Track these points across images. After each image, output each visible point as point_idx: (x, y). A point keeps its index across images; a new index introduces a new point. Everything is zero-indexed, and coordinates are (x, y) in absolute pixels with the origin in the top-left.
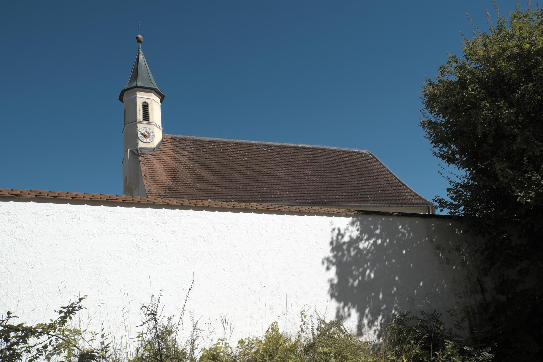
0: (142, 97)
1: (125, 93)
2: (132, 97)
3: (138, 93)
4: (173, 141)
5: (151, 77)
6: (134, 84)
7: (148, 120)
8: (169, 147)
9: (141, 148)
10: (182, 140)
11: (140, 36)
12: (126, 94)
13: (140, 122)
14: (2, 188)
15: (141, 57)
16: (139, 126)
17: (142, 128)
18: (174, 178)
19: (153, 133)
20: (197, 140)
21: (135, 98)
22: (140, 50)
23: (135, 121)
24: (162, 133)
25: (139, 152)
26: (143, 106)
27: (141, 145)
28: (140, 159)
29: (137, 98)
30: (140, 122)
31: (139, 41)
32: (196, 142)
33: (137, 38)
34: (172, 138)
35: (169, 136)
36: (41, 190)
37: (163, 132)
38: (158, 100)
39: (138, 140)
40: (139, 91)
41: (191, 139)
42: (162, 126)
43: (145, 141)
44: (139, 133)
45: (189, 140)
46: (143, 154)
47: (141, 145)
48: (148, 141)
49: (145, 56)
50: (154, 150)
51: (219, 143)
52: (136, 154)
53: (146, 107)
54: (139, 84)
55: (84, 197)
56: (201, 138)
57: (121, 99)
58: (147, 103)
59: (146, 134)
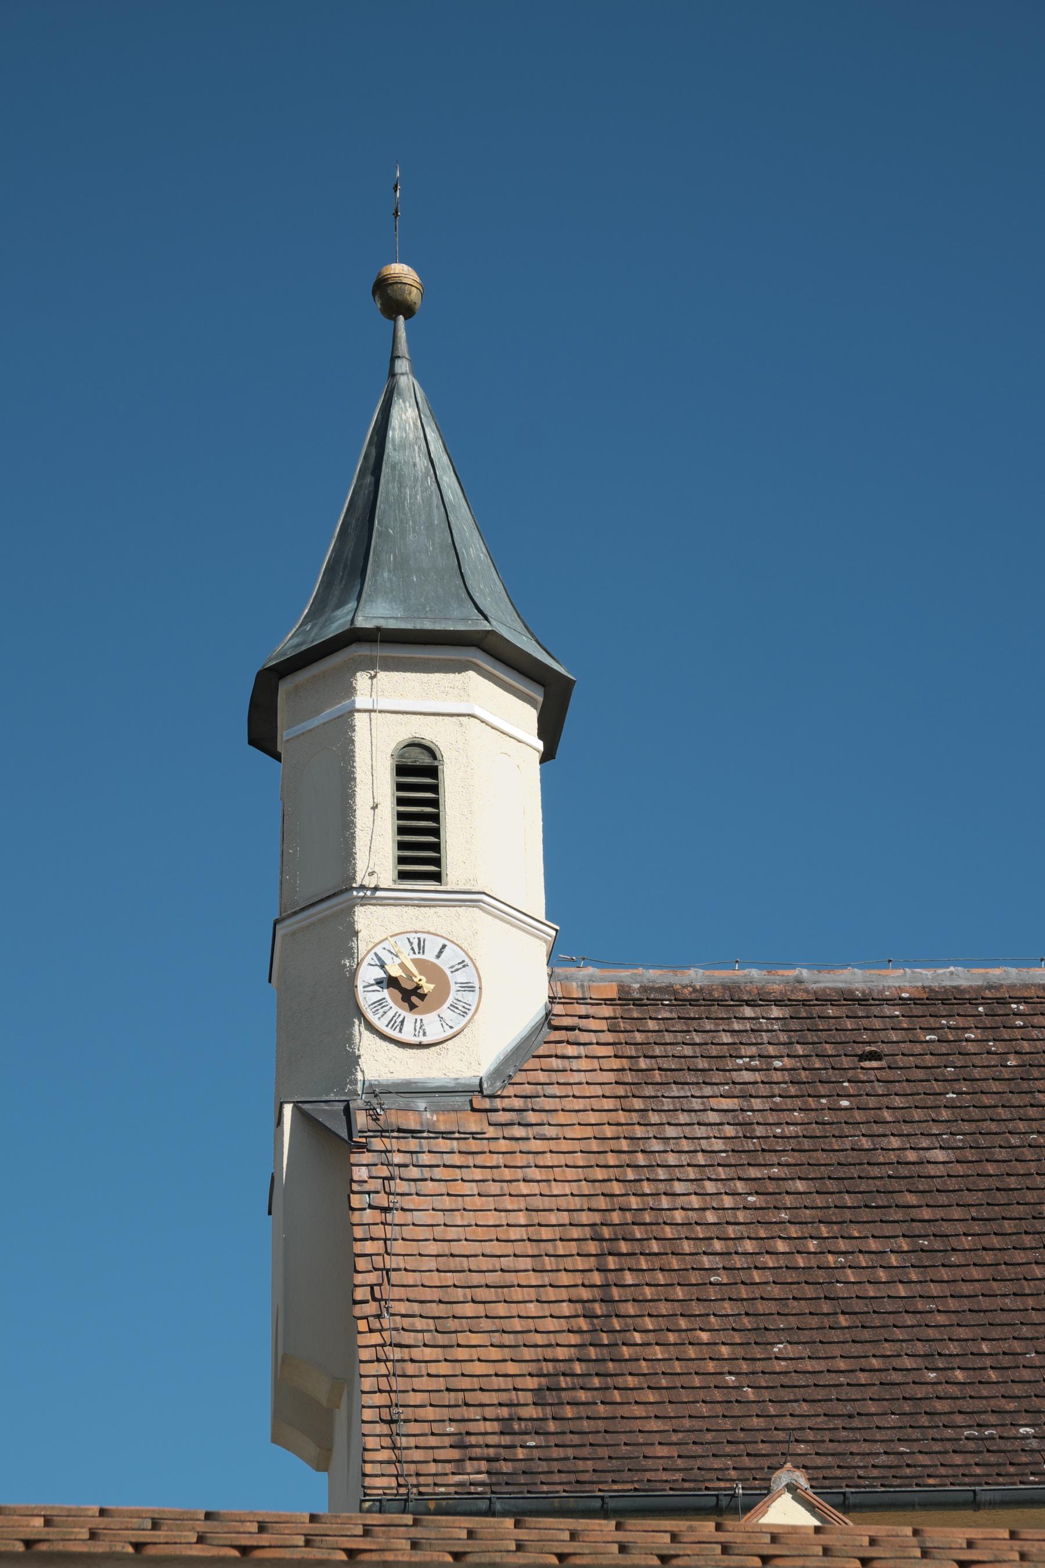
0: (389, 708)
1: (284, 687)
2: (329, 713)
3: (362, 680)
4: (640, 1028)
5: (475, 551)
6: (338, 624)
7: (437, 877)
8: (590, 1067)
9: (377, 1091)
10: (702, 1000)
11: (400, 270)
12: (282, 702)
13: (372, 895)
14: (3, 1504)
15: (405, 416)
16: (370, 922)
17: (384, 934)
18: (601, 1311)
19: (473, 963)
20: (823, 999)
21: (344, 724)
22: (402, 366)
23: (341, 892)
24: (552, 959)
25: (361, 1120)
26: (401, 770)
27: (377, 1063)
28: (360, 1173)
29: (360, 721)
30: (372, 895)
31: (391, 302)
32: (806, 1010)
33: (383, 287)
34: (624, 998)
35: (601, 980)
36: (266, 1510)
37: (557, 957)
38: (520, 717)
39: (358, 1028)
40: (370, 665)
41: (776, 988)
42: (551, 913)
43: (407, 1036)
44: (368, 974)
45: (761, 1000)
46: (382, 1133)
47: (377, 1063)
48: (434, 1031)
49: (442, 410)
50: (475, 1096)
51: (997, 1002)
52: (334, 1134)
53: (419, 776)
54: (376, 612)
55: (623, 1548)
56: (854, 978)
57: (263, 734)
58: (430, 751)
59: (421, 979)
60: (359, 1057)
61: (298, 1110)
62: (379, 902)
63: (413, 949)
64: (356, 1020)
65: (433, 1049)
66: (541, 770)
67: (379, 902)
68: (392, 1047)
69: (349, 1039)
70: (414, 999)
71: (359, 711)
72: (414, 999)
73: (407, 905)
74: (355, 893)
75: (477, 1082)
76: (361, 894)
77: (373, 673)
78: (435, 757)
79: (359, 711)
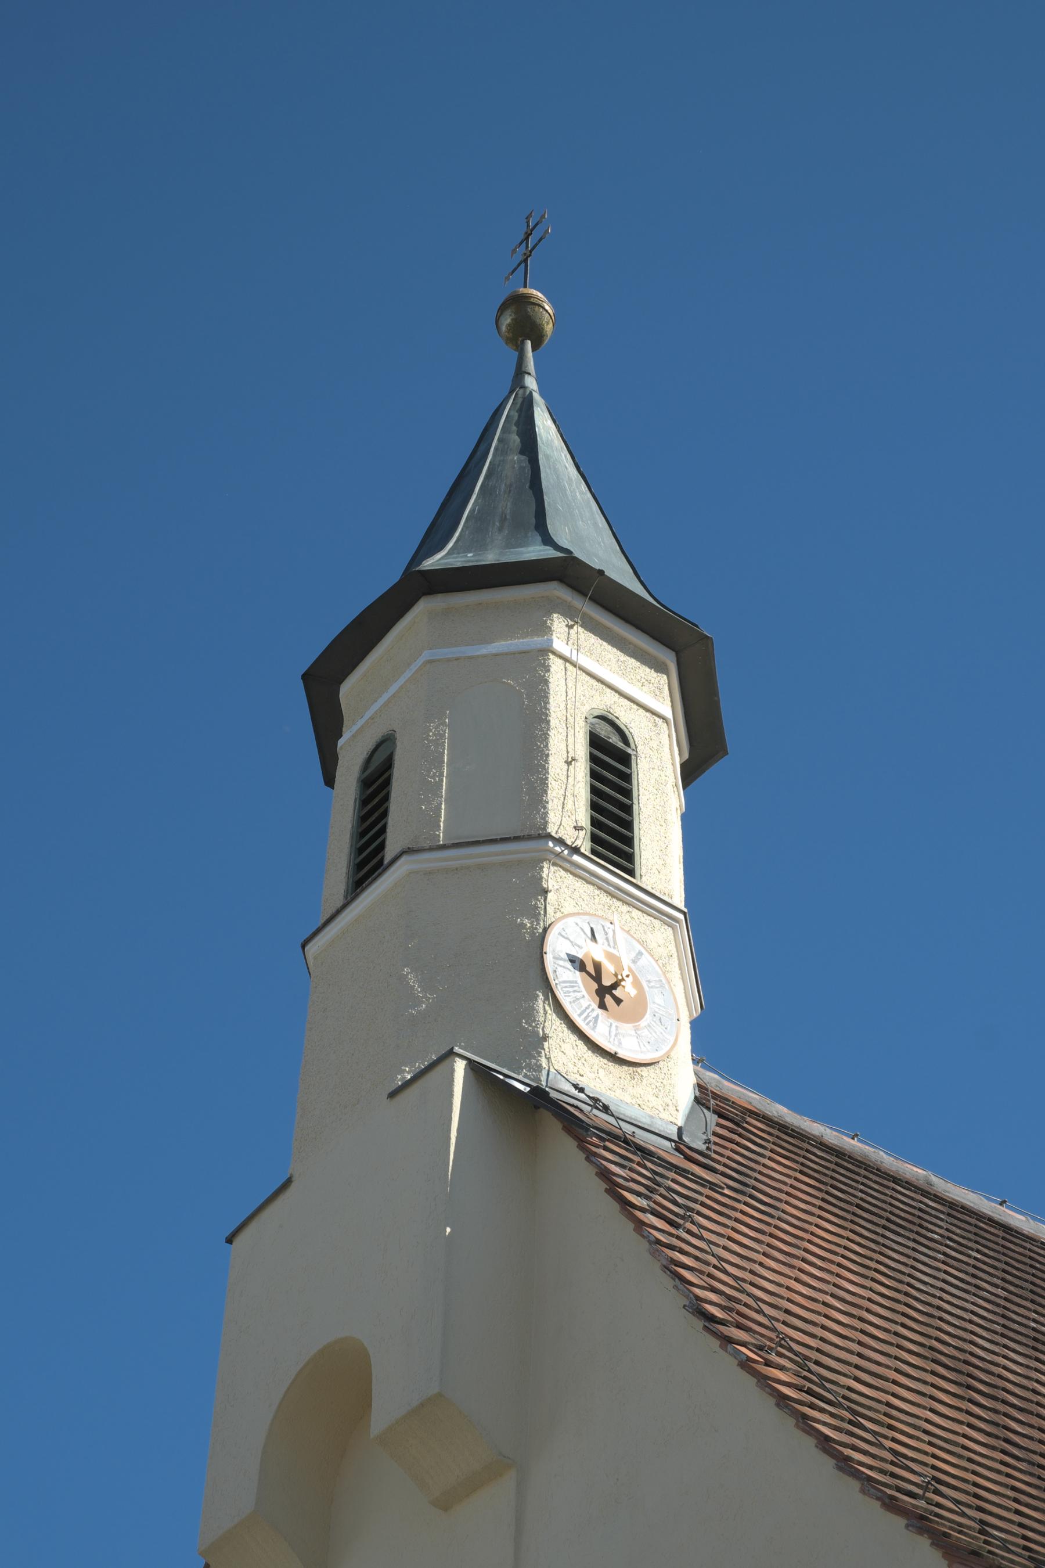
33: (519, 303)
60: (545, 1038)
61: (477, 1071)
62: (573, 869)
63: (607, 939)
64: (540, 994)
65: (625, 1068)
66: (688, 821)
67: (573, 869)
68: (582, 1046)
69: (530, 1014)
70: (608, 999)
71: (554, 653)
72: (608, 999)
73: (599, 888)
74: (551, 844)
75: (675, 1130)
76: (558, 849)
77: (571, 623)
78: (626, 742)
79: (554, 653)
